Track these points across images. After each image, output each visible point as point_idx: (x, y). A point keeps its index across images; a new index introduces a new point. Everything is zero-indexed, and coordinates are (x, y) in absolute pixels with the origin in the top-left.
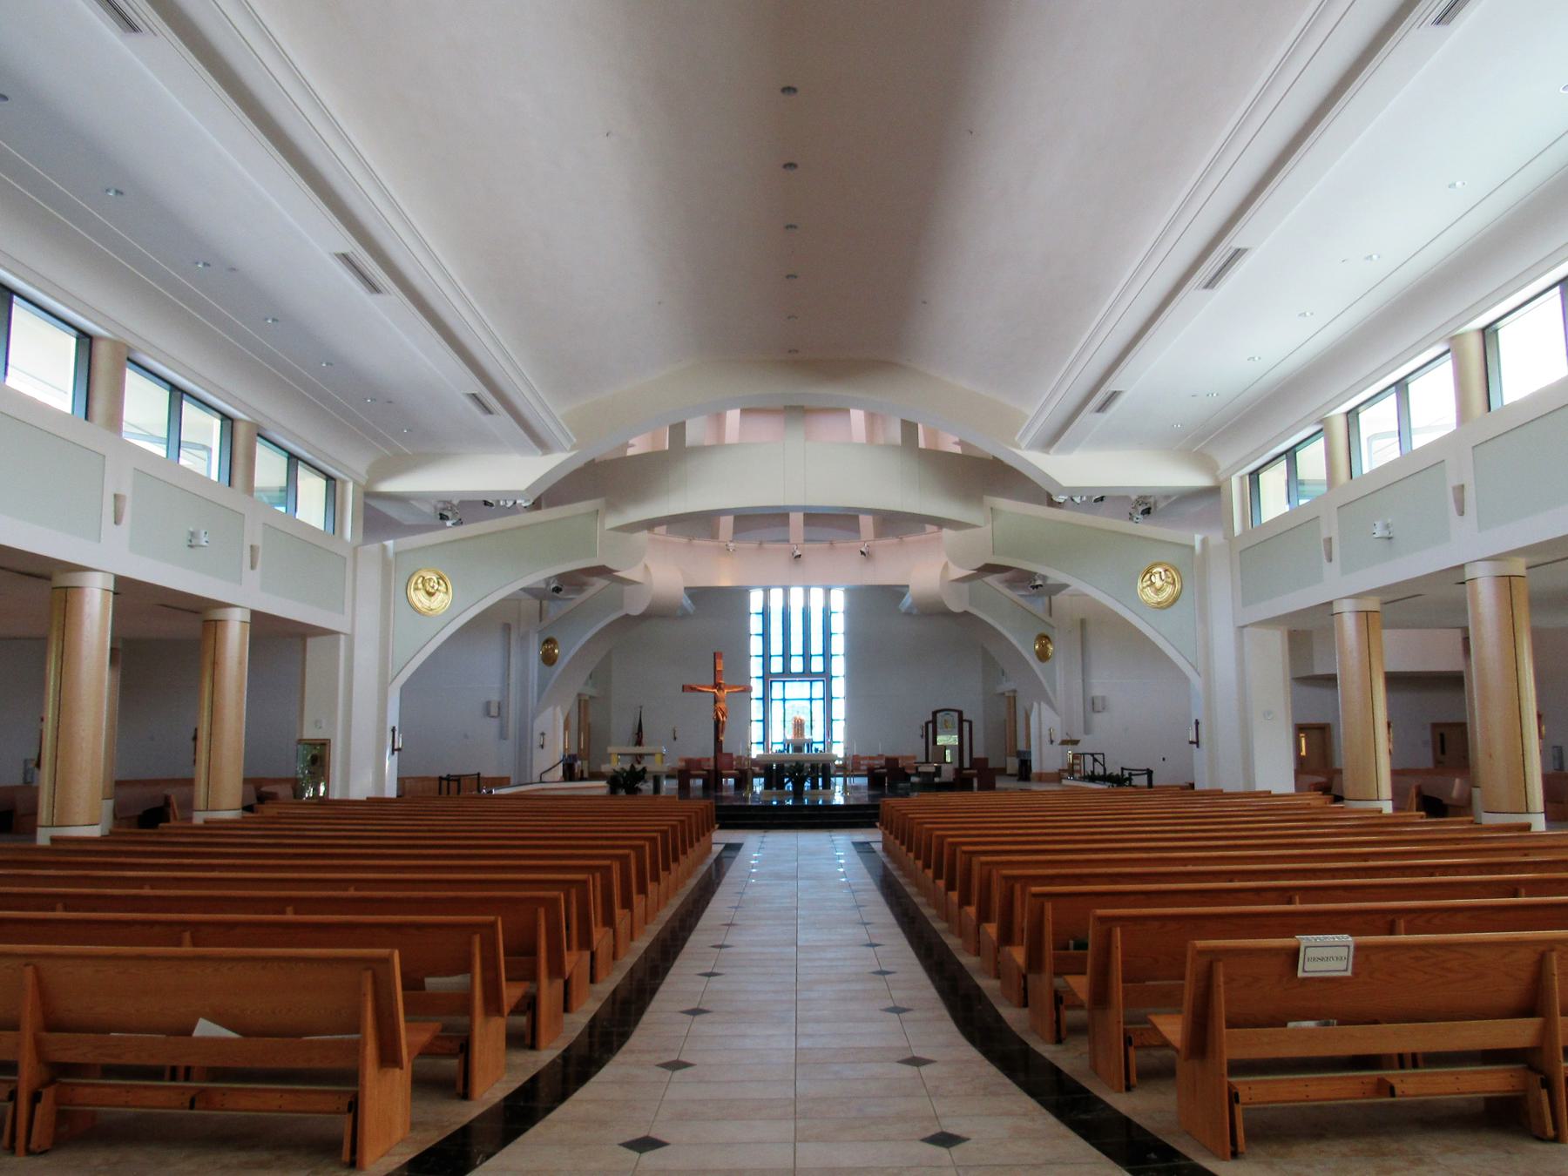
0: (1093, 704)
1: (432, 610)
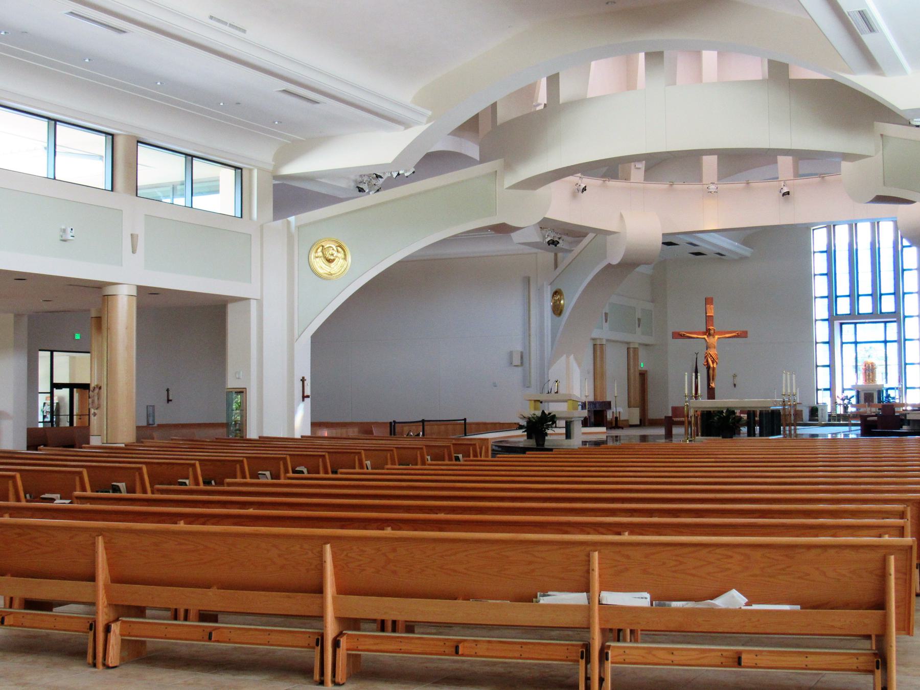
1: (331, 275)
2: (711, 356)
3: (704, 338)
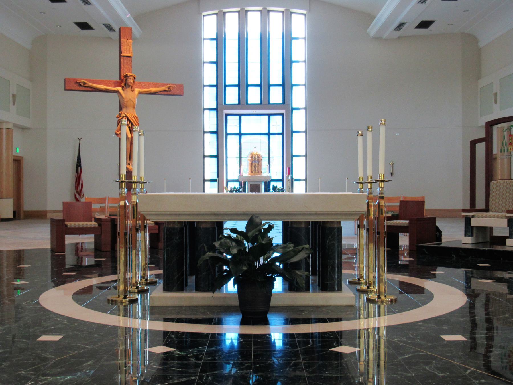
2: (128, 119)
3: (117, 92)
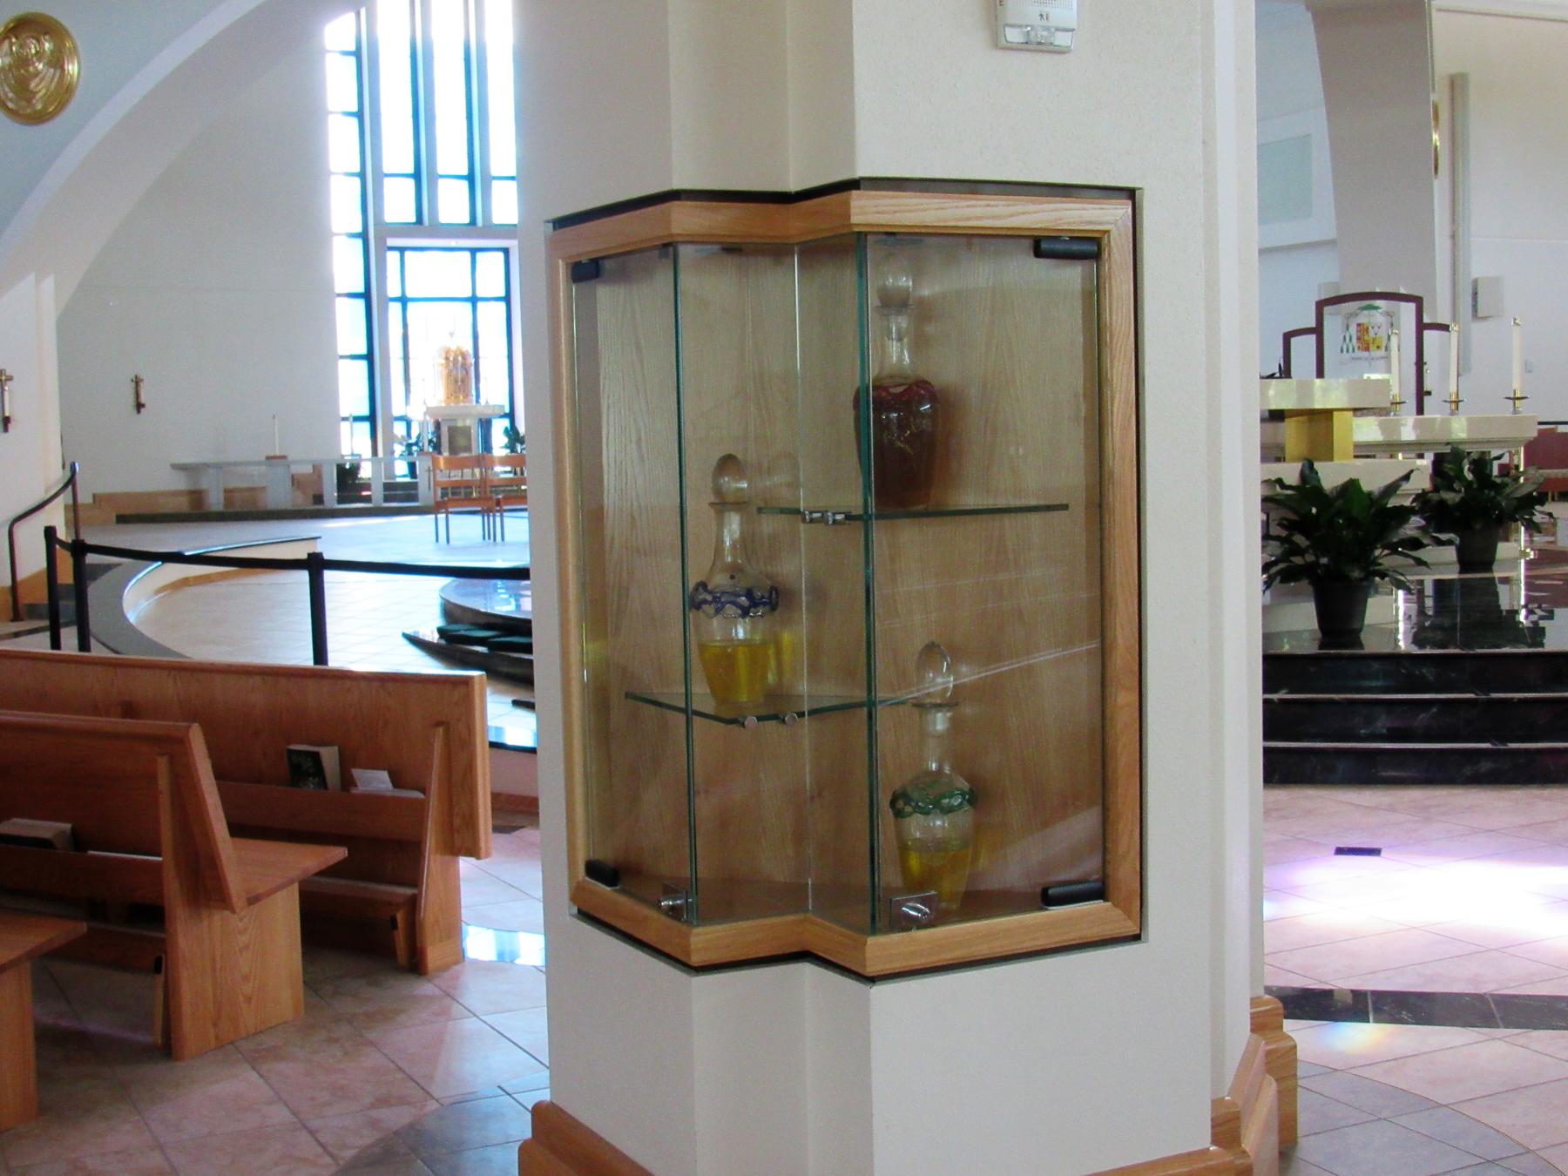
0: (1475, 294)
